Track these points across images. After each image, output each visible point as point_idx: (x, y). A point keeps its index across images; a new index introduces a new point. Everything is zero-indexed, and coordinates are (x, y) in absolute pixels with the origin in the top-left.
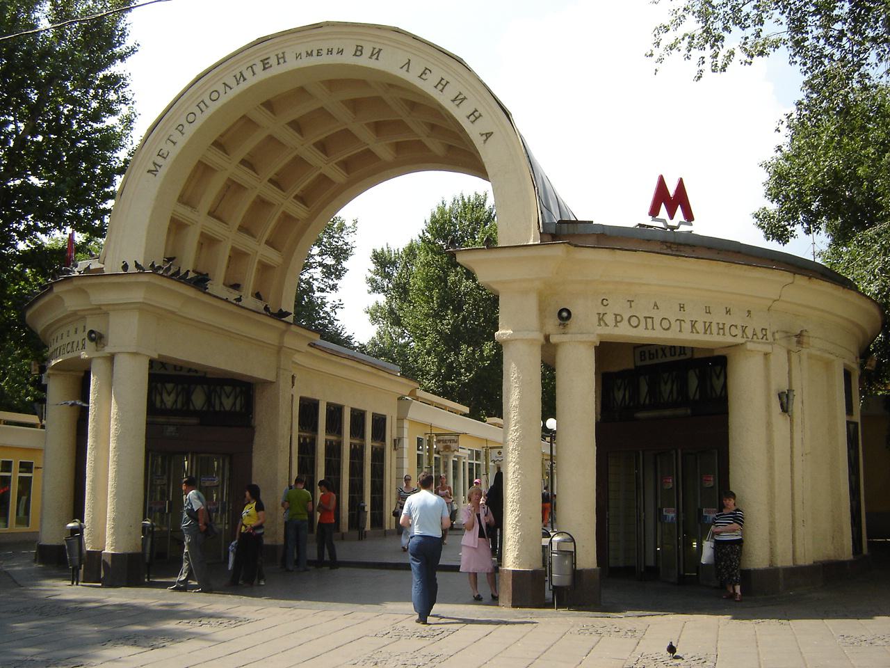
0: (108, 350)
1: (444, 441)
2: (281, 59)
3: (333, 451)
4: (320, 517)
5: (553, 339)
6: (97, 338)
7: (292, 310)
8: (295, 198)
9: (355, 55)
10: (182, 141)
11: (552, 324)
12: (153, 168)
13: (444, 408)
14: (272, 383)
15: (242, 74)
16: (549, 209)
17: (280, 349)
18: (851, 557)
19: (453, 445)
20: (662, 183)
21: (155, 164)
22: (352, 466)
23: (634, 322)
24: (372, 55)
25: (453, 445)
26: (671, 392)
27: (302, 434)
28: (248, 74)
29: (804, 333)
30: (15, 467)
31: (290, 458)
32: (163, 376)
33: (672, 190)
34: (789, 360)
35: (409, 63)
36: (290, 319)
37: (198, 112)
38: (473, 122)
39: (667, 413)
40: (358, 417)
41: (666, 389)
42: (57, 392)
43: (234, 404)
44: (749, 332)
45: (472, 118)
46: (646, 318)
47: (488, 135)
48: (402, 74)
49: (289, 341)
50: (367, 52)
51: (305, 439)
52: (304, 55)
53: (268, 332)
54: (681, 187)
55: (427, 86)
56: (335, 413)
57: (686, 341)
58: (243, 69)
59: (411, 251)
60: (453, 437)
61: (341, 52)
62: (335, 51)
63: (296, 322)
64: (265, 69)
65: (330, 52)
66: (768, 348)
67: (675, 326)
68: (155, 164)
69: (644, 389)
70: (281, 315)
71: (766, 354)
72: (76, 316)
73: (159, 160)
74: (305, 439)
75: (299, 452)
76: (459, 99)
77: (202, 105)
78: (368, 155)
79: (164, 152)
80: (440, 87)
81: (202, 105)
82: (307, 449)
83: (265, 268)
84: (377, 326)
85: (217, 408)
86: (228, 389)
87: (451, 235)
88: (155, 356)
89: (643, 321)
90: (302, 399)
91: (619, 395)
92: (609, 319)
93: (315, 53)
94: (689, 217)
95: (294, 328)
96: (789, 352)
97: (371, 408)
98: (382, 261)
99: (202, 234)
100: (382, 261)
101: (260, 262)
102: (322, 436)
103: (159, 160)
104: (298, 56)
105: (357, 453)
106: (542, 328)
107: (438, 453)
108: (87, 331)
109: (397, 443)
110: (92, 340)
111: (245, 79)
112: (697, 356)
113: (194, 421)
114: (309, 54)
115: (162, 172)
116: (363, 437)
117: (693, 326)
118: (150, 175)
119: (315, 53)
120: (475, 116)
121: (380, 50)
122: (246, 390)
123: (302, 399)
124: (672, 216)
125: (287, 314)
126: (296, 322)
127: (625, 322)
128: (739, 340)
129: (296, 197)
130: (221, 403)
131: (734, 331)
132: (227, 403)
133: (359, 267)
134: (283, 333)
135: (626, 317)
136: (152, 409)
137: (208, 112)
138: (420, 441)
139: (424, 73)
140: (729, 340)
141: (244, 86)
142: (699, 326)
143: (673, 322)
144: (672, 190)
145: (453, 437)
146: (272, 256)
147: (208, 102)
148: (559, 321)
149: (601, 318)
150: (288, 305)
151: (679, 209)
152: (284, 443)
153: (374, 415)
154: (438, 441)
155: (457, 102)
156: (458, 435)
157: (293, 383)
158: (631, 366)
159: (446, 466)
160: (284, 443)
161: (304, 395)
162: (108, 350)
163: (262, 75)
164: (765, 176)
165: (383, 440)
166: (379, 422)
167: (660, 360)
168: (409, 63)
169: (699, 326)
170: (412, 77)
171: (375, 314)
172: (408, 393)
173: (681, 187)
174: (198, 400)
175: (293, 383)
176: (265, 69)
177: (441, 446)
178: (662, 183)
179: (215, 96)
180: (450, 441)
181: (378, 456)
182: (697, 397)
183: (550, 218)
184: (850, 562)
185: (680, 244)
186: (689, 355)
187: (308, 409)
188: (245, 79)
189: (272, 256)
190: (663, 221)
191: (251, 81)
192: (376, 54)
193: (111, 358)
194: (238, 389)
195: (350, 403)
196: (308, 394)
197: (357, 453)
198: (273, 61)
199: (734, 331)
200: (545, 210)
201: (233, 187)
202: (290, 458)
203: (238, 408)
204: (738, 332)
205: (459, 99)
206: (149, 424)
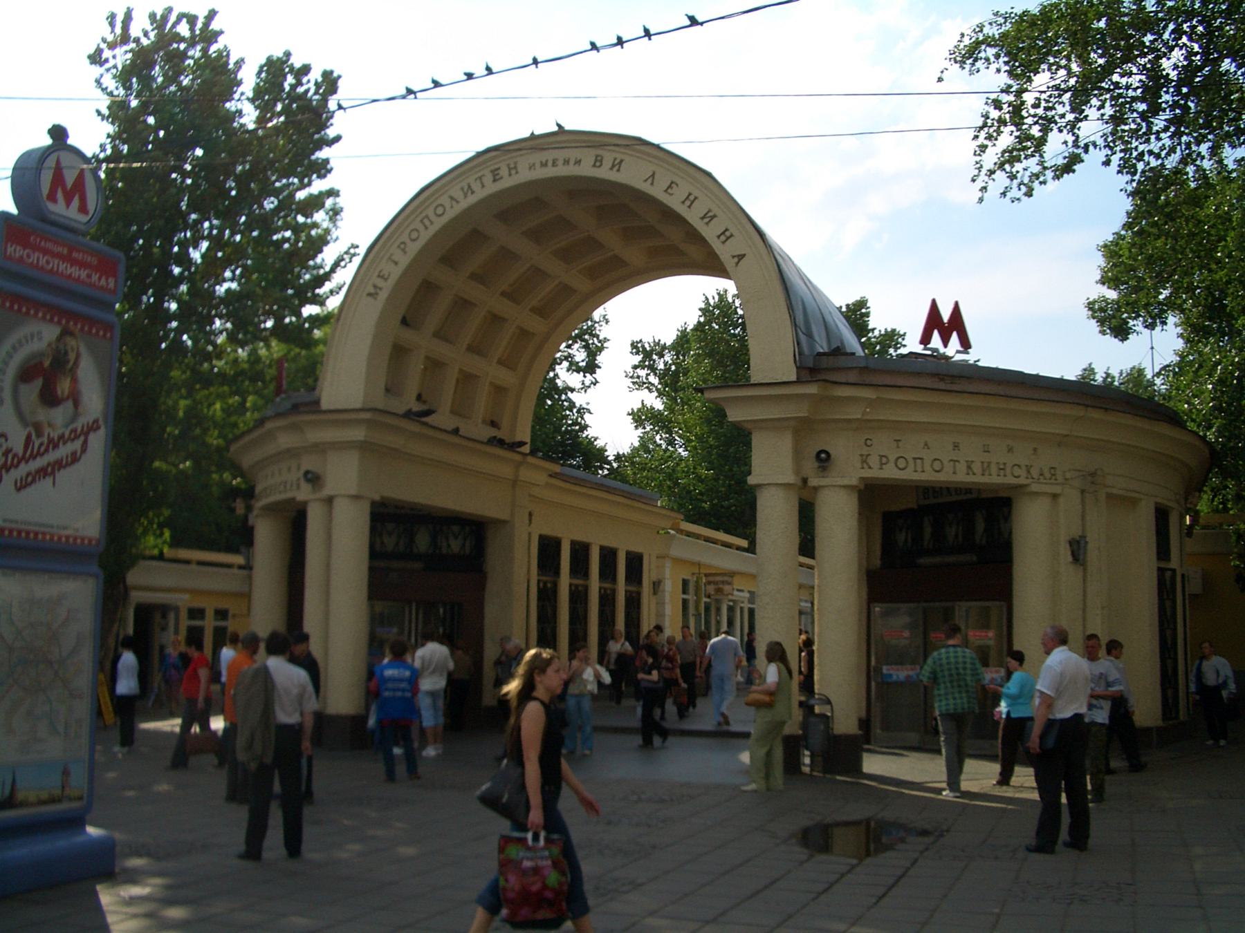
0: (327, 491)
1: (716, 583)
2: (513, 169)
3: (579, 598)
4: (272, 783)
5: (813, 482)
6: (314, 479)
7: (528, 440)
8: (531, 310)
9: (594, 165)
10: (404, 261)
11: (810, 466)
12: (372, 290)
13: (714, 542)
14: (504, 522)
15: (469, 187)
16: (809, 335)
17: (515, 483)
18: (1160, 723)
19: (727, 588)
20: (934, 306)
21: (375, 286)
22: (602, 613)
23: (901, 463)
24: (613, 166)
25: (727, 588)
26: (957, 536)
27: (544, 578)
28: (476, 186)
29: (1099, 473)
30: (210, 614)
31: (528, 606)
32: (389, 519)
33: (946, 315)
34: (1083, 502)
35: (653, 175)
36: (526, 449)
37: (421, 228)
38: (724, 242)
39: (951, 559)
40: (608, 556)
41: (951, 532)
42: (267, 535)
43: (397, 544)
44: (1035, 473)
45: (723, 238)
46: (915, 459)
47: (741, 257)
48: (645, 187)
49: (526, 474)
50: (607, 163)
51: (545, 583)
52: (538, 165)
53: (501, 465)
54: (956, 312)
55: (674, 202)
56: (580, 552)
57: (962, 482)
58: (471, 180)
59: (683, 342)
60: (726, 578)
61: (578, 162)
62: (572, 162)
63: (533, 452)
64: (494, 181)
65: (567, 162)
66: (1057, 490)
67: (948, 467)
68: (375, 286)
69: (928, 531)
70: (515, 446)
71: (1055, 496)
72: (292, 453)
73: (380, 283)
74: (545, 583)
75: (539, 599)
76: (709, 217)
77: (426, 221)
78: (617, 261)
79: (385, 273)
80: (688, 203)
81: (426, 221)
82: (547, 596)
83: (499, 390)
84: (640, 430)
85: (444, 551)
86: (456, 528)
87: (715, 347)
88: (377, 498)
89: (911, 462)
90: (541, 537)
91: (901, 537)
92: (874, 461)
93: (550, 163)
94: (966, 344)
95: (530, 459)
96: (1083, 492)
97: (624, 545)
98: (646, 353)
99: (427, 358)
100: (646, 353)
101: (491, 383)
102: (565, 581)
103: (380, 283)
104: (532, 167)
105: (607, 600)
106: (797, 471)
107: (709, 597)
108: (302, 472)
109: (657, 585)
110: (308, 480)
111: (473, 192)
112: (984, 496)
113: (418, 565)
114: (544, 165)
115: (383, 295)
116: (586, 575)
117: (969, 467)
118: (370, 299)
119: (550, 163)
120: (725, 236)
121: (622, 161)
122: (477, 530)
123: (541, 537)
124: (946, 343)
125: (522, 444)
126: (533, 452)
127: (892, 464)
128: (1022, 481)
129: (533, 310)
130: (449, 546)
131: (1017, 471)
132: (455, 546)
133: (616, 361)
134: (518, 465)
135: (892, 458)
136: (374, 554)
137: (433, 230)
138: (685, 583)
139: (670, 187)
140: (1011, 480)
141: (472, 199)
142: (977, 467)
143: (945, 463)
144: (946, 315)
145: (726, 578)
146: (505, 377)
147: (433, 218)
148: (816, 464)
149: (864, 460)
150: (524, 433)
151: (955, 336)
152: (520, 590)
153: (628, 553)
154: (709, 583)
155: (706, 220)
156: (732, 574)
157: (530, 520)
158: (914, 506)
159: (718, 610)
160: (520, 590)
161: (544, 532)
162: (327, 491)
163: (492, 188)
164: (1100, 260)
165: (640, 583)
166: (635, 562)
167: (955, 498)
168: (653, 175)
169: (977, 467)
170: (657, 191)
171: (640, 417)
172: (670, 525)
173: (956, 312)
174: (422, 542)
175: (530, 520)
176: (494, 181)
177: (711, 589)
178: (934, 306)
179: (440, 211)
180: (723, 582)
181: (634, 603)
182: (984, 542)
183: (812, 347)
184: (1158, 729)
185: (953, 376)
186: (974, 496)
187: (548, 549)
188: (473, 192)
189: (505, 377)
190: (936, 350)
191: (480, 194)
192: (617, 165)
193: (330, 501)
194: (467, 528)
195: (597, 539)
196: (547, 531)
197: (607, 600)
198: (504, 172)
199: (1017, 471)
200: (803, 338)
201: (467, 379)
202: (528, 606)
203: (468, 551)
204: (1023, 472)
205: (709, 217)
206: (371, 569)
